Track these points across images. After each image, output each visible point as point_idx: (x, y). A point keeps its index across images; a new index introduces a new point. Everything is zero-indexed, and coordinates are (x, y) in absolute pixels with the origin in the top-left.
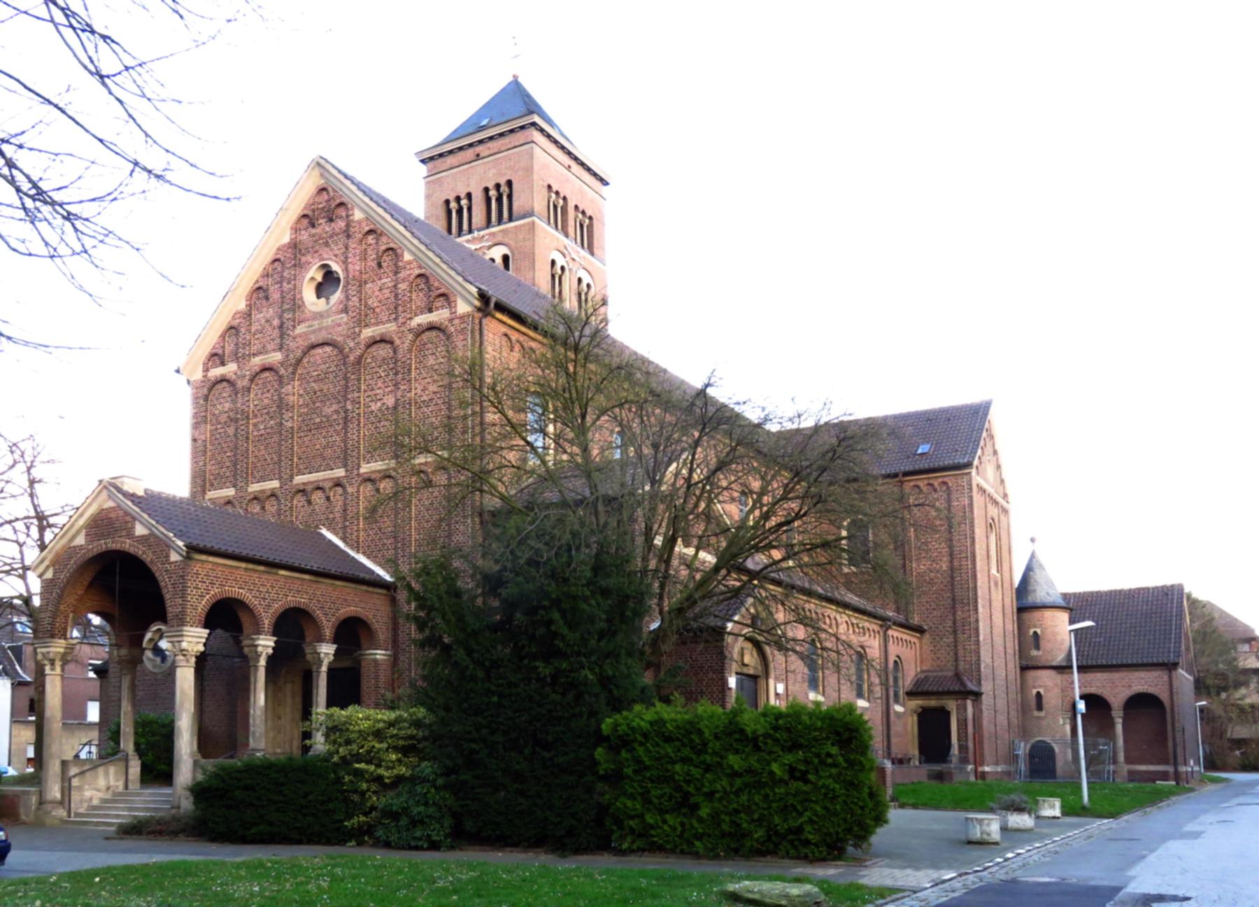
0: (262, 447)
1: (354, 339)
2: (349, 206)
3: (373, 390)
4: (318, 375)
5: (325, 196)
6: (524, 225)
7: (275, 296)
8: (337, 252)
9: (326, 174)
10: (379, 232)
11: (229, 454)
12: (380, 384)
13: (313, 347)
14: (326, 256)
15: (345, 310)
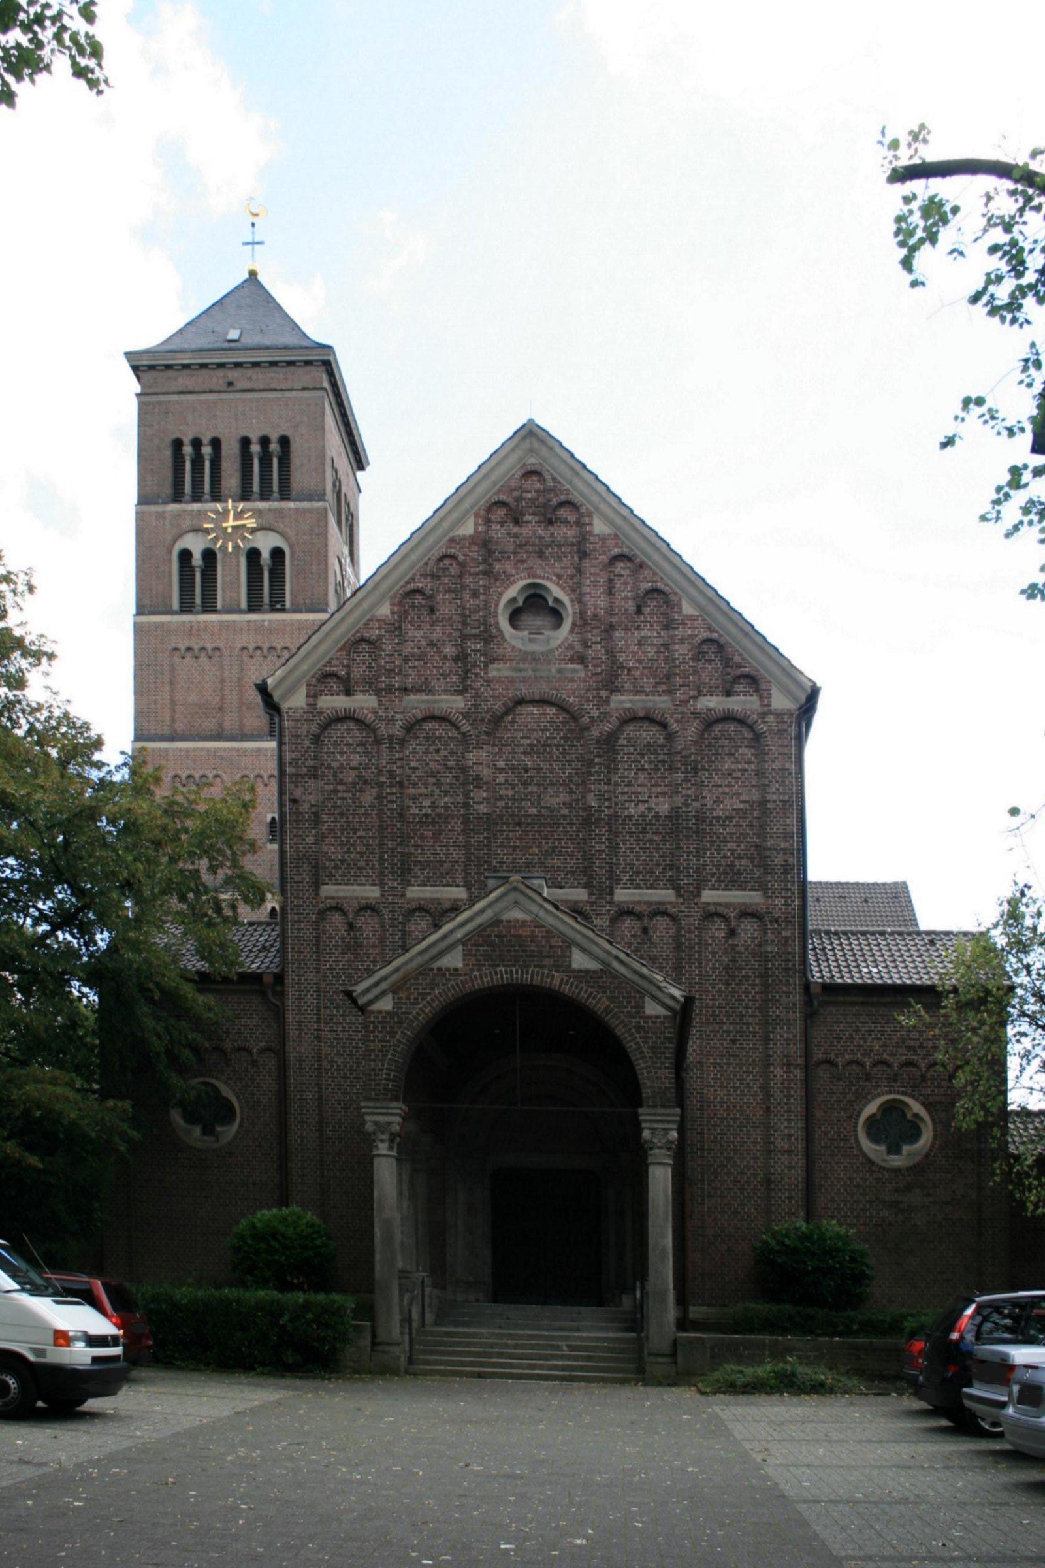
3: (629, 784)
5: (534, 484)
6: (310, 511)
7: (446, 609)
13: (520, 702)
14: (539, 572)
15: (581, 660)
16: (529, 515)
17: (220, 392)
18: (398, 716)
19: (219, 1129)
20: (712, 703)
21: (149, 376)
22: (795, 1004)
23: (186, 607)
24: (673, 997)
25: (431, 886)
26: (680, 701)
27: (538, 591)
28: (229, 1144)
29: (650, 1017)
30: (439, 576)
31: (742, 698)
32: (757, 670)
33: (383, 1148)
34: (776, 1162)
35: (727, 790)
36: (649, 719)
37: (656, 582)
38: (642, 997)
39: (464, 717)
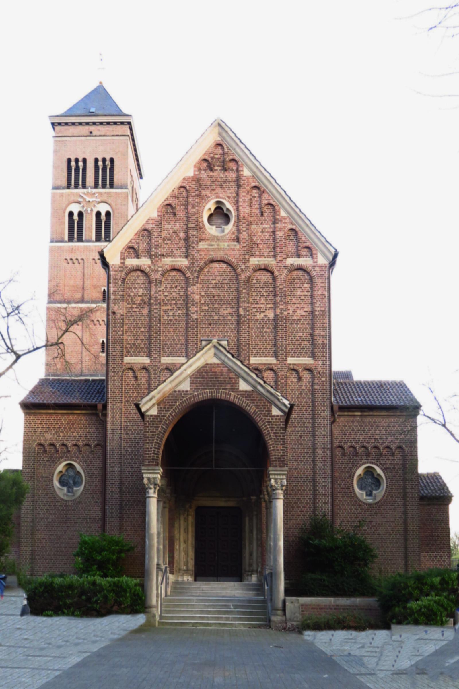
0: (171, 330)
1: (245, 263)
2: (240, 163)
3: (257, 304)
4: (216, 284)
6: (121, 193)
7: (181, 214)
8: (230, 195)
9: (224, 134)
10: (262, 189)
11: (142, 330)
12: (263, 301)
13: (212, 261)
14: (221, 195)
15: (238, 240)
16: (218, 166)
17: (86, 136)
18: (160, 269)
19: (75, 489)
20: (291, 261)
21: (58, 128)
22: (327, 416)
23: (71, 239)
24: (285, 405)
25: (172, 357)
26: (280, 260)
27: (220, 205)
28: (79, 497)
29: (274, 416)
30: (178, 197)
31: (305, 259)
32: (312, 244)
33: (151, 491)
34: (319, 501)
35: (298, 305)
36: (266, 269)
37: (269, 200)
38: (271, 406)
39: (188, 269)
